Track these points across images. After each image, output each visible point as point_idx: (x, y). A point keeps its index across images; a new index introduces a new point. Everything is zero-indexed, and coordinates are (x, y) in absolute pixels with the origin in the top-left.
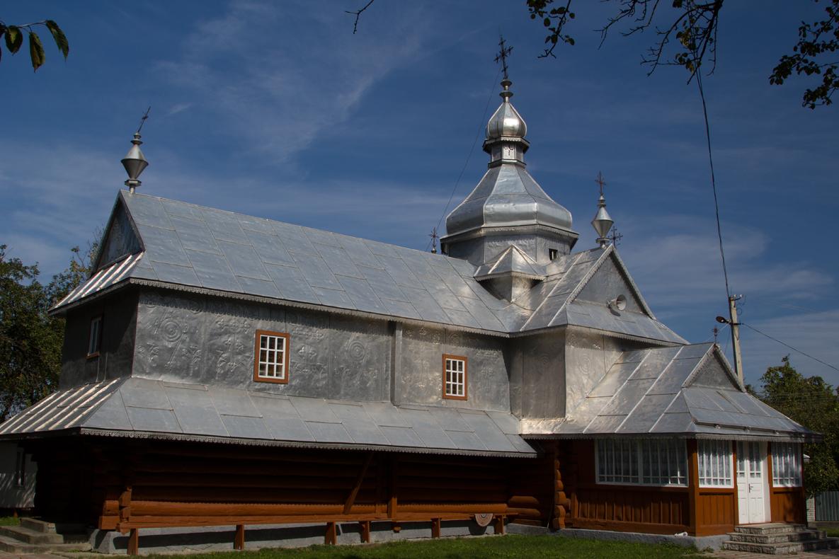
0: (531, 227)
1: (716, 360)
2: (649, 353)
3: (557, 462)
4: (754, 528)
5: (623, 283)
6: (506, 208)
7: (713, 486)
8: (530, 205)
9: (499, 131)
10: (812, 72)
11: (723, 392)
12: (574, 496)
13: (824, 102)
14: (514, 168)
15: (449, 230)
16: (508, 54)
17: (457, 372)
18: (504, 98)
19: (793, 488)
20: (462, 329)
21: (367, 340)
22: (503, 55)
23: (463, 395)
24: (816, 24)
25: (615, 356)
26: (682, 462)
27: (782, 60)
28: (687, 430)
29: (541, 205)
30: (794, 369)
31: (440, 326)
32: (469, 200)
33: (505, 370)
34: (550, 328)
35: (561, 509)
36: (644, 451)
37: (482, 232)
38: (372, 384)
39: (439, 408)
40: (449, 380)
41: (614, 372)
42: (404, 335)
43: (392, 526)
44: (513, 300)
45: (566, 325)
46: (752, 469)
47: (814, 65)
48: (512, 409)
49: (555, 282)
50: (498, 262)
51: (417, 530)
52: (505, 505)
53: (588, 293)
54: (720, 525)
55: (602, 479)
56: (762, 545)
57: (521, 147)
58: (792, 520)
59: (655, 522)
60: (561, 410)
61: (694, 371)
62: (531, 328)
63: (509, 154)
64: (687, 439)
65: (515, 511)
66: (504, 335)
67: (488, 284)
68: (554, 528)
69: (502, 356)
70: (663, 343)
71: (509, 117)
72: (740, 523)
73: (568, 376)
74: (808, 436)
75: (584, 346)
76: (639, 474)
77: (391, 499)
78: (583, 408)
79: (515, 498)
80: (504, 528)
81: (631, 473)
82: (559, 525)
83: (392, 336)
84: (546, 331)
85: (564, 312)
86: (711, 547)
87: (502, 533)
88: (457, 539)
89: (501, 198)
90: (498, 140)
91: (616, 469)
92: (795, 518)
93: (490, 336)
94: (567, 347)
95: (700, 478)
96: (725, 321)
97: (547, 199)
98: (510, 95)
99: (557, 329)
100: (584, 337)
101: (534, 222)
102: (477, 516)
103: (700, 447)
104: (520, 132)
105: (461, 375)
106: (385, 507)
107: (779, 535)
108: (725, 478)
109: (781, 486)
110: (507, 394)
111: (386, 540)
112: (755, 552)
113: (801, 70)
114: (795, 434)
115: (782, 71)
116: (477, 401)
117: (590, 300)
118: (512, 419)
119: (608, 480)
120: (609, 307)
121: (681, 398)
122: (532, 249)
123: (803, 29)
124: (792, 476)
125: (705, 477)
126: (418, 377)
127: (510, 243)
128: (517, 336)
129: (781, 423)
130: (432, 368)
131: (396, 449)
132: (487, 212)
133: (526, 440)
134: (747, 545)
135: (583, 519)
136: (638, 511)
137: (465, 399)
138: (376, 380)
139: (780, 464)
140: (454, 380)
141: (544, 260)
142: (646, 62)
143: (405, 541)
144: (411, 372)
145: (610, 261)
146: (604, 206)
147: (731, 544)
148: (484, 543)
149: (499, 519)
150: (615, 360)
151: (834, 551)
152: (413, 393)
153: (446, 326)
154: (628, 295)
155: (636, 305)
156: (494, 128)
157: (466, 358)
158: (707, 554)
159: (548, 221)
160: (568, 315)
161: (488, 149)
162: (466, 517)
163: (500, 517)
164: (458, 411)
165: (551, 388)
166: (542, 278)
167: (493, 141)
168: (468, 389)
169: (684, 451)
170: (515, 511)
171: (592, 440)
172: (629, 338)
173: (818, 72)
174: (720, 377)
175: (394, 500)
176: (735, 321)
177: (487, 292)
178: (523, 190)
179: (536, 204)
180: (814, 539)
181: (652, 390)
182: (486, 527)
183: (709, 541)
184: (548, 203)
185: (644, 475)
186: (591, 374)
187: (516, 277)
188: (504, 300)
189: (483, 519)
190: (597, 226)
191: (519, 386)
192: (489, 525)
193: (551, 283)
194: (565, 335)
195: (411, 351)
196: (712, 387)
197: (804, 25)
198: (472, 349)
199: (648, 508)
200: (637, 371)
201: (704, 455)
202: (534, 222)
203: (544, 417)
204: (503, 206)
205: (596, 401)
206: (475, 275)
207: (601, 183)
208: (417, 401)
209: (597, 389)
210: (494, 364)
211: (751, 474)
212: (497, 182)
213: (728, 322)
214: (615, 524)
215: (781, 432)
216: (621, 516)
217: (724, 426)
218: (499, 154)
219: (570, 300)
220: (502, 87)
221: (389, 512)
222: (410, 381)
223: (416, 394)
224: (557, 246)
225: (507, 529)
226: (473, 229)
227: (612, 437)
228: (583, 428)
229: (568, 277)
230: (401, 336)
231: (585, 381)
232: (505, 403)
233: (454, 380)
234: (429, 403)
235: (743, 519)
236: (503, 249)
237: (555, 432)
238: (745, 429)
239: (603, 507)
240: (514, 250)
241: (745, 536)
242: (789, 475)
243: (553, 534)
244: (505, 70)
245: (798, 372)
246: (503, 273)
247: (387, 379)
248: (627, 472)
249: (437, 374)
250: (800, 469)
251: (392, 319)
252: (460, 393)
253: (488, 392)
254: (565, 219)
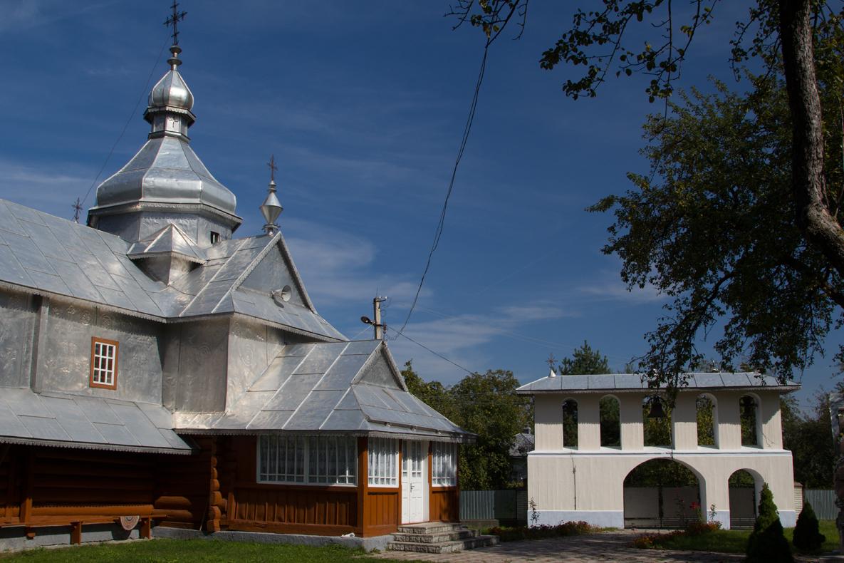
0: (193, 206)
1: (382, 358)
2: (312, 348)
3: (214, 460)
4: (418, 528)
5: (287, 273)
6: (168, 183)
7: (380, 485)
8: (194, 182)
9: (164, 100)
10: (580, 62)
11: (387, 390)
12: (232, 496)
13: (588, 94)
14: (177, 142)
15: (100, 200)
16: (180, 19)
17: (107, 357)
18: (172, 65)
19: (449, 487)
20: (116, 310)
21: (7, 316)
22: (175, 19)
23: (112, 384)
24: (591, 14)
25: (277, 349)
26: (352, 461)
27: (557, 44)
28: (359, 428)
29: (207, 184)
30: (415, 374)
31: (92, 305)
32: (125, 171)
33: (159, 358)
34: (214, 314)
35: (217, 509)
36: (311, 449)
37: (139, 207)
38: (9, 367)
39: (84, 396)
40: (97, 366)
41: (277, 365)
42: (51, 312)
43: (25, 532)
44: (170, 283)
45: (232, 313)
46: (414, 469)
47: (582, 55)
48: (164, 401)
49: (217, 267)
50: (156, 240)
51: (53, 536)
52: (151, 506)
53: (252, 282)
54: (385, 525)
55: (263, 478)
56: (428, 544)
57: (187, 121)
58: (446, 519)
59: (329, 523)
60: (221, 404)
61: (363, 368)
62: (192, 314)
63: (172, 126)
64: (358, 438)
65: (162, 513)
66: (160, 320)
67: (141, 263)
68: (208, 531)
69: (156, 343)
70: (325, 339)
71: (176, 86)
72: (403, 522)
73: (230, 368)
74: (466, 437)
75: (247, 336)
76: (305, 472)
77: (25, 500)
78: (244, 403)
79: (163, 499)
80: (151, 532)
81: (295, 471)
82: (214, 527)
83: (36, 312)
84: (209, 318)
85: (230, 298)
86: (378, 548)
87: (148, 537)
88: (101, 545)
89: (159, 172)
90: (161, 109)
91: (279, 467)
92: (449, 517)
93: (145, 320)
94: (230, 337)
95: (369, 477)
96: (369, 322)
97: (211, 179)
98: (179, 63)
99: (222, 317)
100: (248, 327)
101: (197, 201)
102: (123, 519)
104: (186, 105)
105: (110, 361)
106: (17, 509)
107: (441, 534)
108: (391, 477)
109: (439, 485)
110: (159, 384)
111: (19, 549)
112: (420, 552)
113: (569, 59)
114: (455, 435)
115: (551, 59)
116: (127, 392)
117: (254, 289)
118: (163, 412)
119: (270, 480)
120: (273, 297)
121: (351, 396)
122: (193, 230)
123: (578, 17)
124: (448, 475)
125: (374, 476)
126: (63, 361)
127: (170, 221)
128: (176, 322)
129: (442, 424)
130: (79, 352)
131: (154, 451)
132: (146, 185)
133: (181, 436)
134: (412, 545)
135: (241, 521)
136: (302, 511)
137: (114, 388)
138: (15, 363)
139: (439, 464)
140: (103, 367)
141: (205, 243)
142: (453, 13)
143: (42, 550)
144: (55, 355)
145: (276, 250)
146: (274, 191)
147: (396, 544)
148: (134, 549)
149: (145, 522)
150: (277, 353)
151: (491, 549)
152: (56, 379)
153: (99, 305)
154: (292, 286)
155: (299, 297)
156: (159, 96)
157: (118, 342)
158: (375, 555)
159: (211, 201)
160: (234, 303)
161: (149, 118)
162: (109, 520)
163: (147, 519)
164: (105, 401)
165: (210, 380)
166: (202, 261)
167: (156, 110)
168: (118, 377)
169: (354, 449)
170: (162, 513)
171: (255, 436)
172: (293, 330)
173: (586, 63)
174: (385, 375)
175: (29, 502)
176: (379, 322)
177: (140, 271)
178: (186, 166)
179: (201, 182)
180: (471, 537)
181: (320, 385)
182: (130, 531)
183: (377, 543)
184: (212, 183)
185: (310, 474)
186: (253, 367)
187: (176, 258)
188: (161, 282)
189: (130, 522)
190: (266, 212)
191: (173, 377)
192: (135, 528)
193: (212, 268)
194: (229, 324)
195: (57, 331)
196: (378, 385)
197: (579, 13)
198: (124, 333)
199: (313, 509)
200: (302, 366)
201: (374, 454)
202: (197, 201)
203: (200, 410)
204: (165, 180)
205: (256, 395)
206: (128, 253)
207: (273, 168)
208: (60, 388)
209: (258, 383)
210: (146, 350)
211: (413, 473)
212: (158, 154)
213: (371, 323)
214: (276, 525)
215: (444, 432)
216: (292, 518)
217: (394, 425)
218: (161, 125)
219: (235, 287)
220: (169, 52)
221: (21, 516)
222: (54, 366)
223: (60, 380)
224: (219, 229)
225: (154, 532)
226: (129, 202)
227: (278, 434)
228: (246, 424)
229: (231, 263)
230: (47, 314)
231: (246, 374)
232: (157, 395)
233: (103, 367)
234: (73, 392)
235: (405, 519)
236: (161, 227)
237: (214, 427)
238: (412, 428)
239: (263, 507)
240: (174, 228)
241: (410, 536)
242: (446, 475)
243: (206, 537)
244: (175, 35)
245: (419, 377)
246: (161, 253)
247: (27, 362)
248: (291, 471)
249: (85, 359)
250: (455, 468)
251: (38, 292)
252: (109, 381)
253: (139, 382)
254: (229, 201)
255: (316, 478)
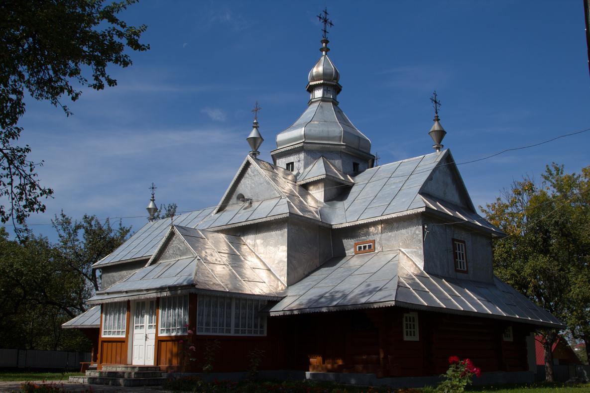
91: (249, 325)
103: (174, 305)
248: (208, 324)
255: (210, 329)
